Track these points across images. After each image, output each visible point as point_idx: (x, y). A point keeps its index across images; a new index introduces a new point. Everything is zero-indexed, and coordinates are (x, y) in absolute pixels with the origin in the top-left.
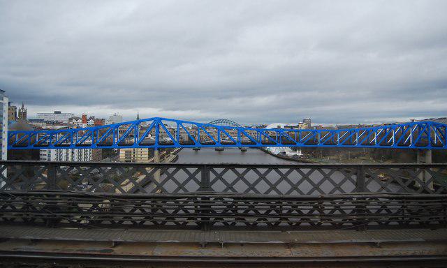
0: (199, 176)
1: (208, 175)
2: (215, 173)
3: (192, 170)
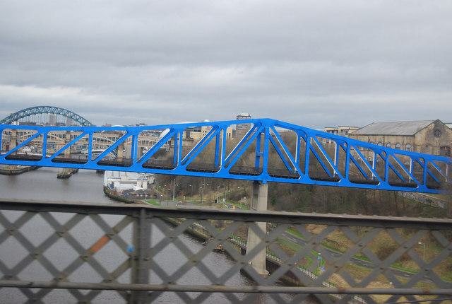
0: (127, 233)
1: (148, 232)
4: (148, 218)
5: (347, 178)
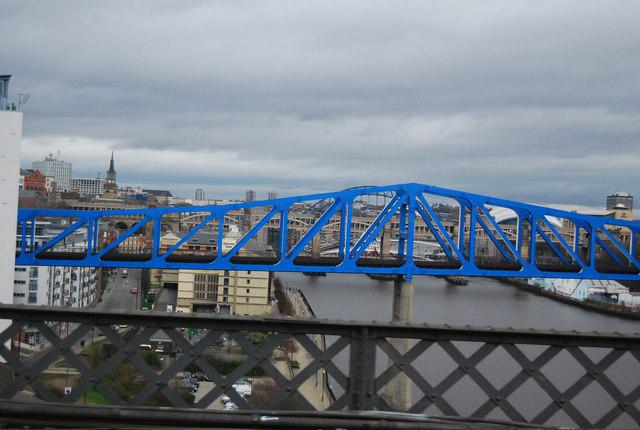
0: (343, 360)
4: (372, 339)
5: (472, 260)
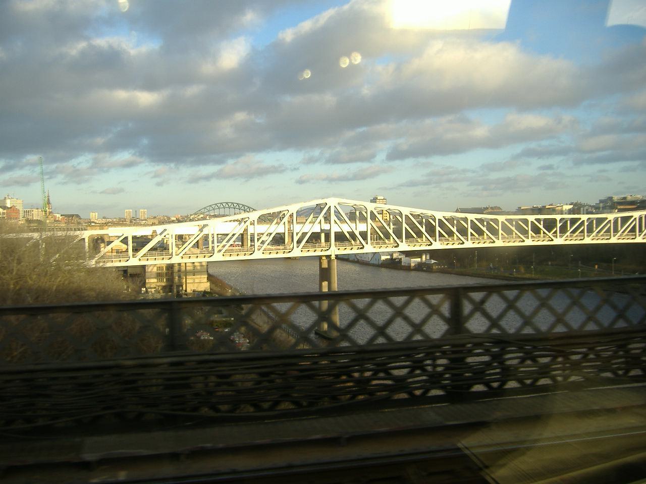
0: (446, 309)
2: (471, 301)
3: (435, 299)
